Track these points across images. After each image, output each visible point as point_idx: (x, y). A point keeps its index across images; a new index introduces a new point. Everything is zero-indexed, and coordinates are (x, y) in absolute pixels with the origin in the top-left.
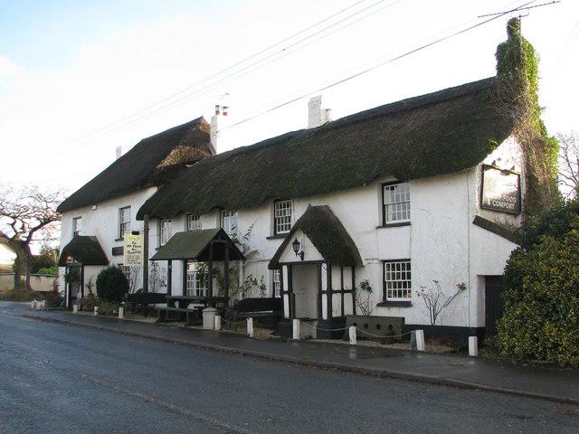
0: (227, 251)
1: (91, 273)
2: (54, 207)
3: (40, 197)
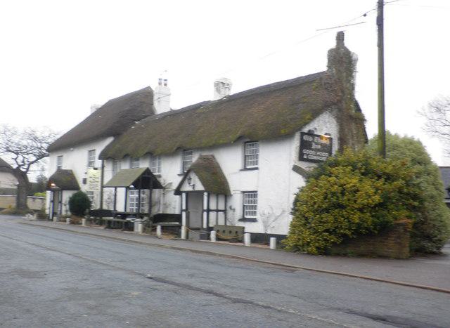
0: (151, 183)
1: (67, 196)
2: (45, 146)
3: (35, 139)
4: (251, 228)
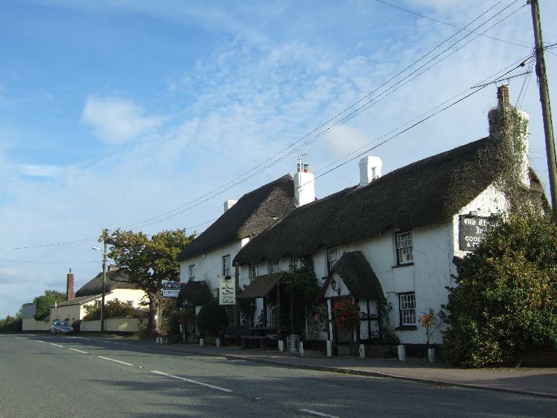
4: (407, 338)
